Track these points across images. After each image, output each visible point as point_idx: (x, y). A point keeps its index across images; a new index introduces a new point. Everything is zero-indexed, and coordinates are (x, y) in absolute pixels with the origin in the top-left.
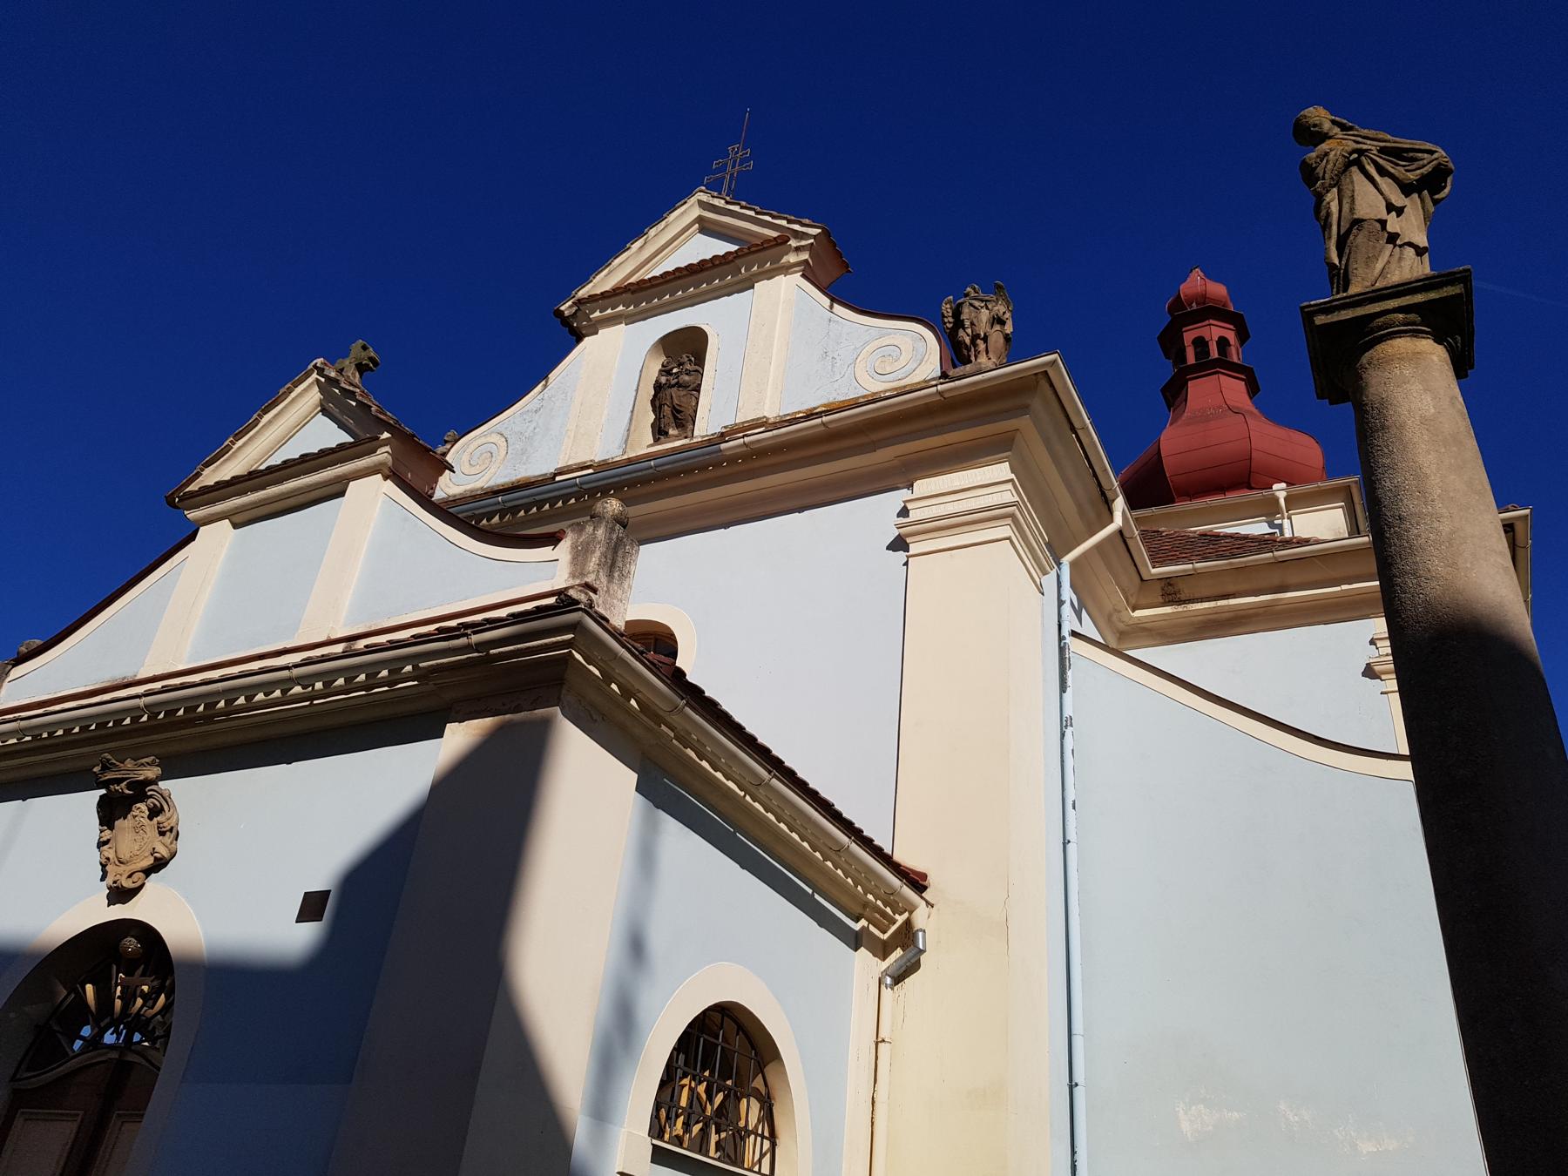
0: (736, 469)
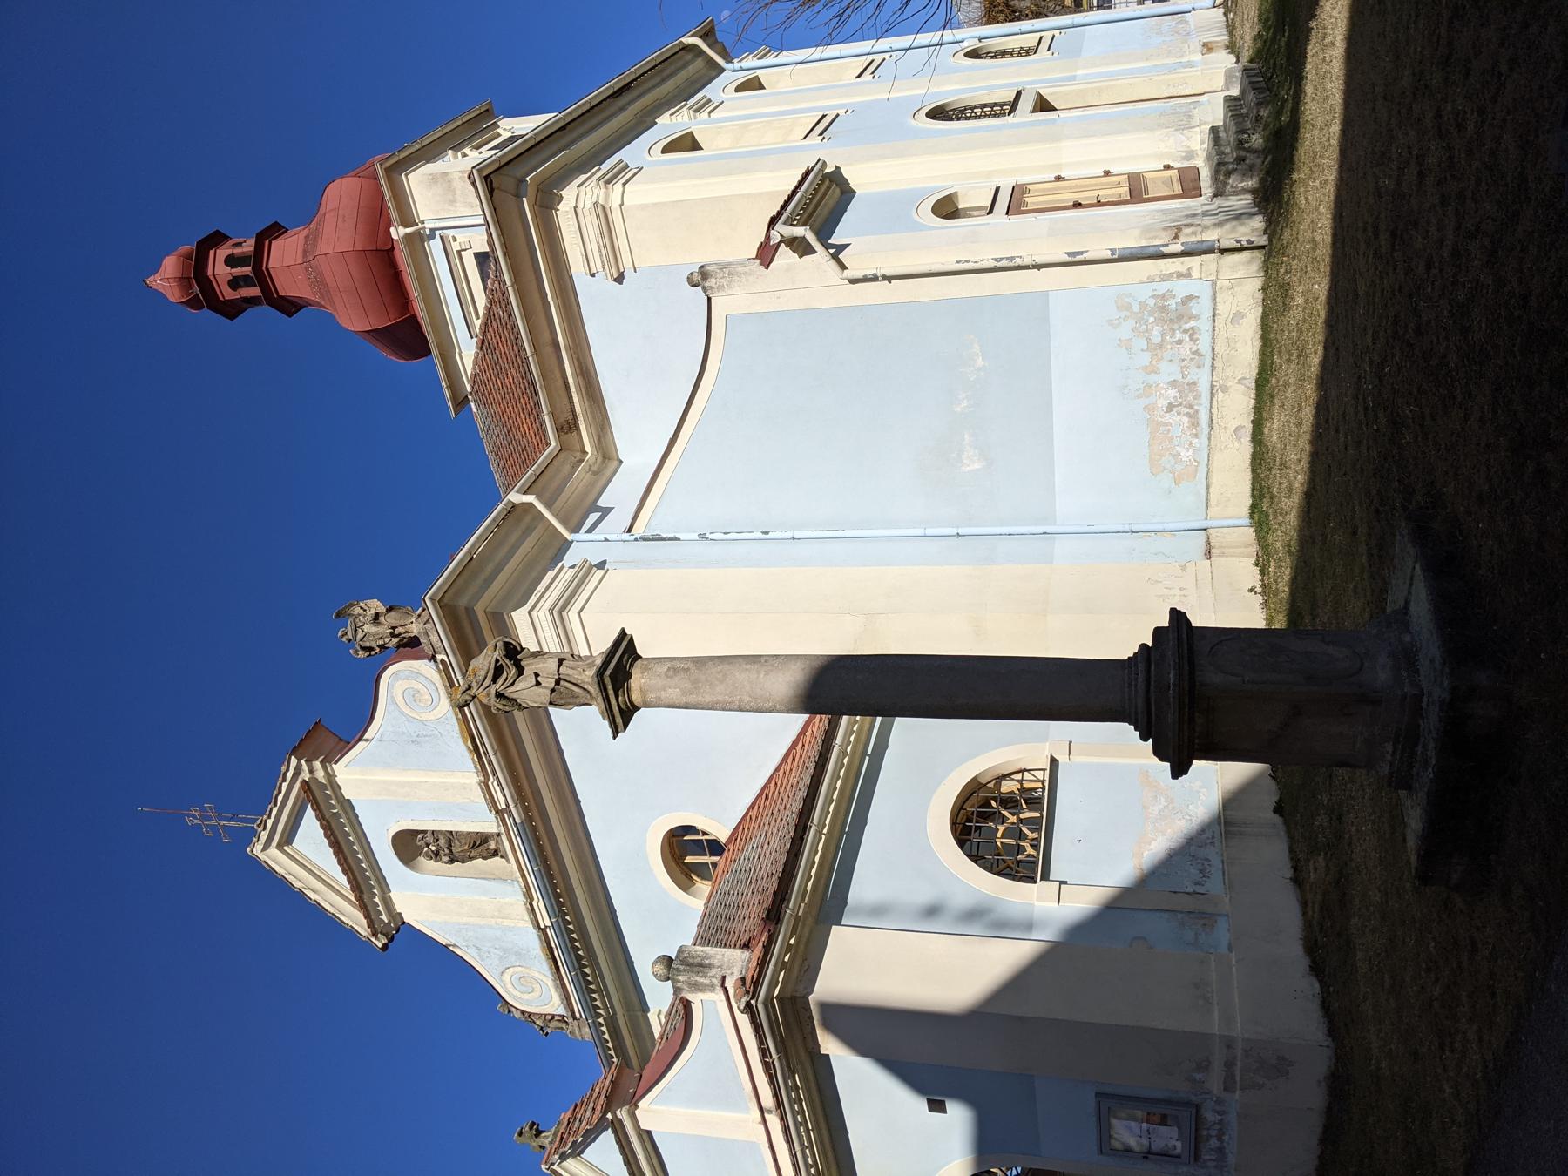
0: (533, 806)
